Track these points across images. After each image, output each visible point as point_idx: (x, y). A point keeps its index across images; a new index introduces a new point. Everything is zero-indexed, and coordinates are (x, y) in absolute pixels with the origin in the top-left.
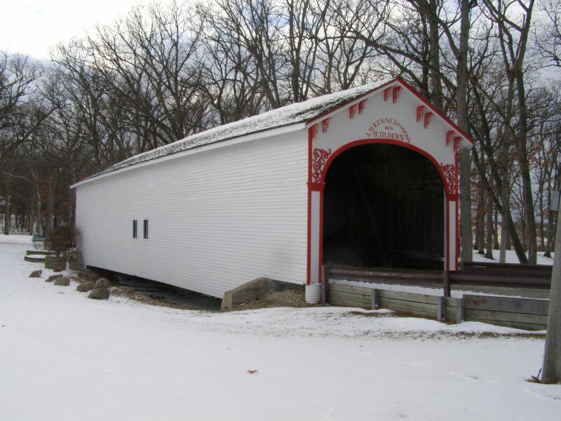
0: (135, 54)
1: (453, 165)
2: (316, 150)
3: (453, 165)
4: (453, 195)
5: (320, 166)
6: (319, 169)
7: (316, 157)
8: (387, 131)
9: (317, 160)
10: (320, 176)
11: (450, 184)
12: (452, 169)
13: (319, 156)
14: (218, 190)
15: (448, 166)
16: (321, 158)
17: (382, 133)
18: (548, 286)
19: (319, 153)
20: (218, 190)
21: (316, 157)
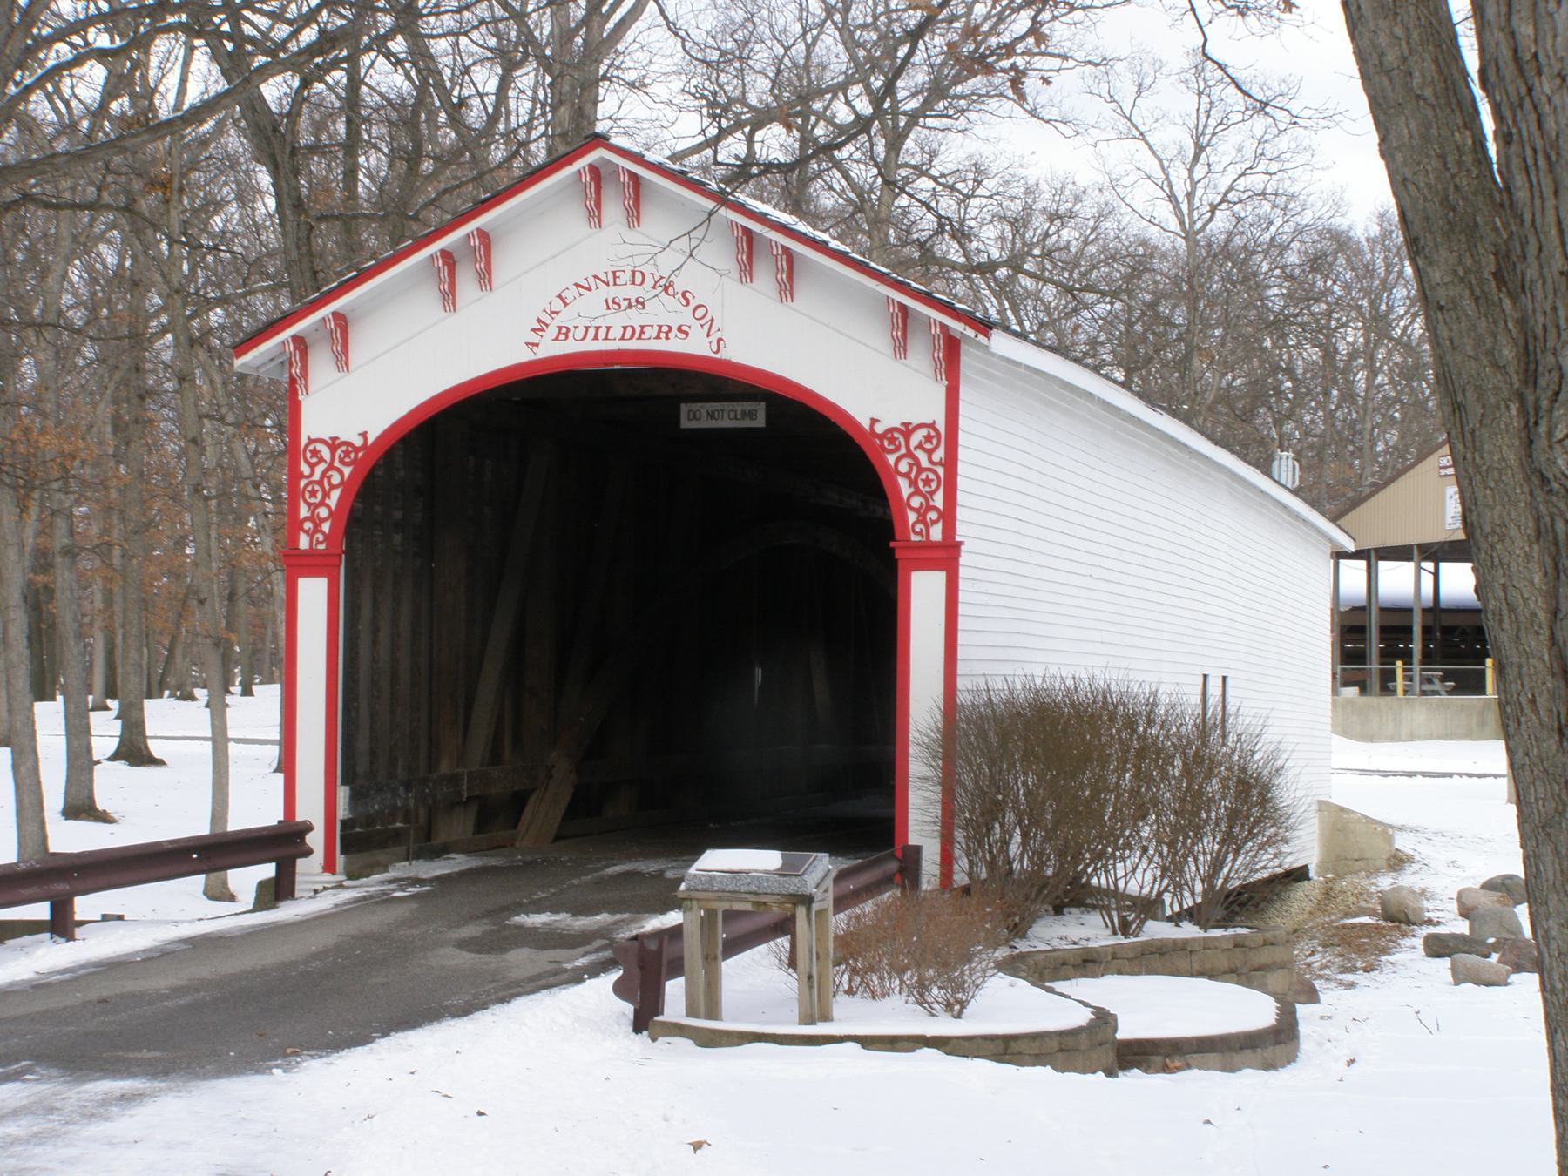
0: (708, 64)
1: (932, 426)
2: (311, 441)
3: (932, 426)
4: (929, 546)
5: (326, 495)
6: (322, 503)
7: (312, 466)
8: (618, 320)
9: (316, 477)
10: (326, 527)
11: (916, 502)
12: (928, 438)
13: (321, 460)
14: (1007, 613)
15: (908, 430)
16: (331, 467)
17: (597, 327)
18: (1457, 984)
19: (325, 452)
20: (1007, 613)
21: (312, 466)
